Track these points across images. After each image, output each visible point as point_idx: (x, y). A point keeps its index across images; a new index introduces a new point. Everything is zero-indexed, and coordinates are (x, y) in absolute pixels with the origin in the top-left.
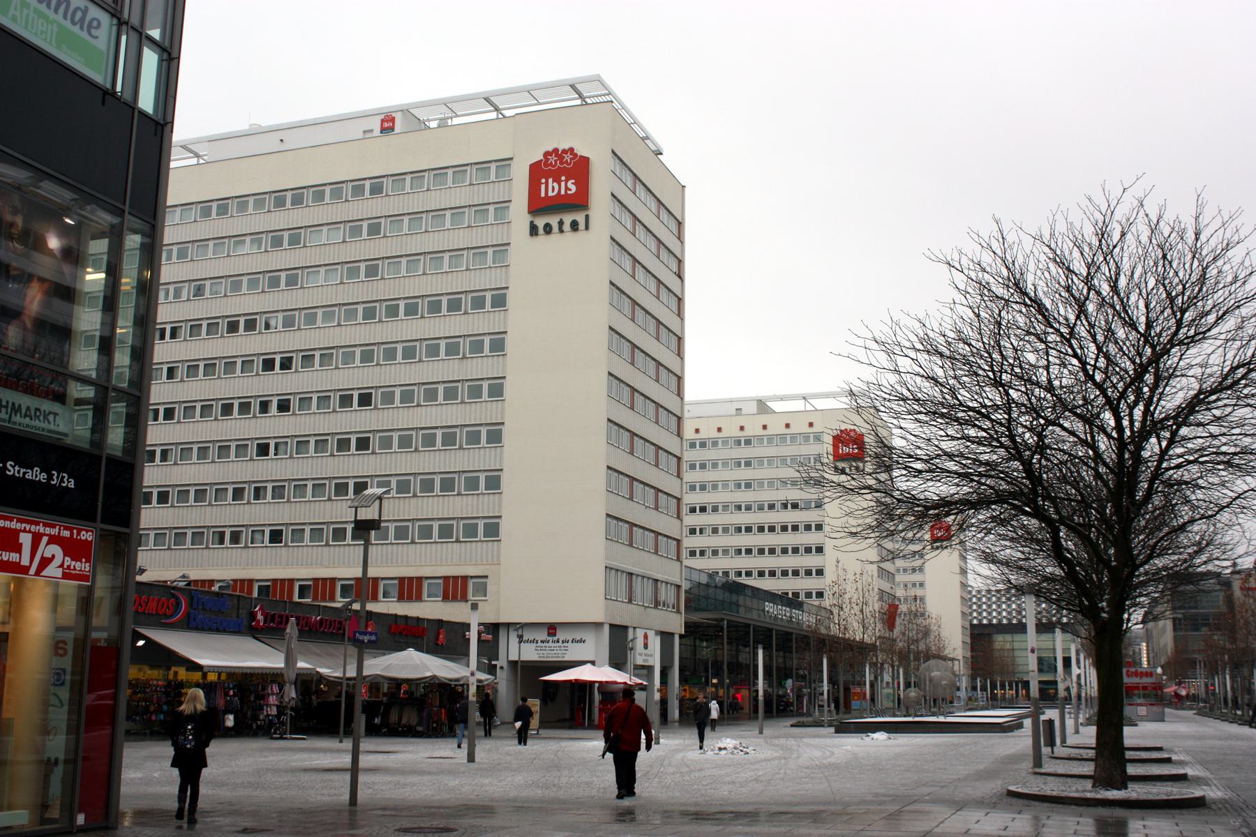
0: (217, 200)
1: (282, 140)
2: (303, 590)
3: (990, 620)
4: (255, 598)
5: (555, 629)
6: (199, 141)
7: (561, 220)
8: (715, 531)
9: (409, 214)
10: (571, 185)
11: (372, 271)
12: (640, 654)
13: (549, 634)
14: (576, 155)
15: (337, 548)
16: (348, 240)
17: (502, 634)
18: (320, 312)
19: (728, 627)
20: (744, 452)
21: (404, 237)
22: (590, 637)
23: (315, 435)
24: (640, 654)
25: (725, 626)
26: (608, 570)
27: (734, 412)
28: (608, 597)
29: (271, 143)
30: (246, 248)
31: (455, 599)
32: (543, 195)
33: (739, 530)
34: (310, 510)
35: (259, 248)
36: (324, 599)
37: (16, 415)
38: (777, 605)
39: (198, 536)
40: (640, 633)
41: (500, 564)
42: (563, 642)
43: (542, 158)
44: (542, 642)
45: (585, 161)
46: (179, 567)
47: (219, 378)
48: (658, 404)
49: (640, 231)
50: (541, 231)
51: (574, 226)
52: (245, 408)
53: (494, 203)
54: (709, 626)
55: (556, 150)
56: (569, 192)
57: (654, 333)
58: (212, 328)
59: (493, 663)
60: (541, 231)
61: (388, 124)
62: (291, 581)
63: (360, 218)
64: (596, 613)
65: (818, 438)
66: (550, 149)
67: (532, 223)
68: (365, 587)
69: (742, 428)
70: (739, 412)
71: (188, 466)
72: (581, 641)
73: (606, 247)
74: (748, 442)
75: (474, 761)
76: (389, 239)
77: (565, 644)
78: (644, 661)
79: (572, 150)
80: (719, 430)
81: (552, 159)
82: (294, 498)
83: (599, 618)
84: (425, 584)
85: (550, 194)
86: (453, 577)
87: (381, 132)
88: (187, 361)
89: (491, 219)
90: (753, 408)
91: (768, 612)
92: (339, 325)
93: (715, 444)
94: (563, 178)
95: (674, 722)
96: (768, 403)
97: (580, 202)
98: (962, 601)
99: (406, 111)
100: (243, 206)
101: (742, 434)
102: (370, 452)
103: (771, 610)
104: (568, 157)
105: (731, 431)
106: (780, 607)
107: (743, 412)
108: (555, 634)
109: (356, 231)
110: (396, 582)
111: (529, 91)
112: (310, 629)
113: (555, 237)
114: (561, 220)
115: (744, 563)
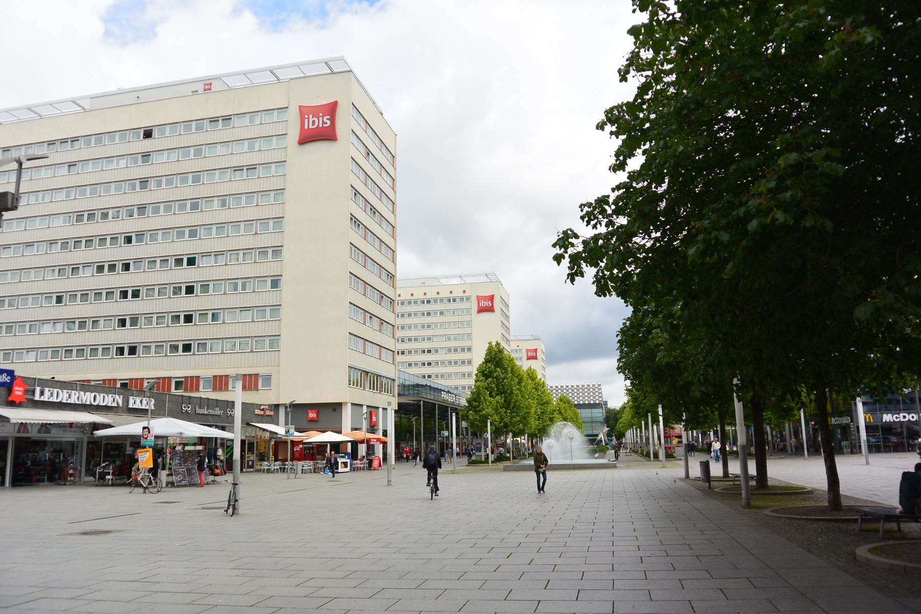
1: (138, 97)
2: (178, 385)
4: (118, 388)
6: (83, 98)
11: (196, 180)
15: (172, 358)
18: (162, 206)
20: (426, 308)
23: (158, 285)
29: (131, 99)
31: (250, 389)
34: (154, 334)
36: (191, 390)
39: (80, 351)
46: (122, 370)
48: (381, 266)
52: (112, 268)
56: (324, 125)
57: (378, 248)
58: (91, 216)
61: (208, 87)
62: (170, 378)
65: (468, 299)
68: (192, 383)
71: (74, 306)
74: (429, 302)
82: (144, 326)
85: (311, 127)
86: (135, 379)
91: (443, 397)
93: (410, 303)
99: (218, 78)
103: (445, 396)
107: (426, 284)
111: (298, 65)
115: (427, 370)
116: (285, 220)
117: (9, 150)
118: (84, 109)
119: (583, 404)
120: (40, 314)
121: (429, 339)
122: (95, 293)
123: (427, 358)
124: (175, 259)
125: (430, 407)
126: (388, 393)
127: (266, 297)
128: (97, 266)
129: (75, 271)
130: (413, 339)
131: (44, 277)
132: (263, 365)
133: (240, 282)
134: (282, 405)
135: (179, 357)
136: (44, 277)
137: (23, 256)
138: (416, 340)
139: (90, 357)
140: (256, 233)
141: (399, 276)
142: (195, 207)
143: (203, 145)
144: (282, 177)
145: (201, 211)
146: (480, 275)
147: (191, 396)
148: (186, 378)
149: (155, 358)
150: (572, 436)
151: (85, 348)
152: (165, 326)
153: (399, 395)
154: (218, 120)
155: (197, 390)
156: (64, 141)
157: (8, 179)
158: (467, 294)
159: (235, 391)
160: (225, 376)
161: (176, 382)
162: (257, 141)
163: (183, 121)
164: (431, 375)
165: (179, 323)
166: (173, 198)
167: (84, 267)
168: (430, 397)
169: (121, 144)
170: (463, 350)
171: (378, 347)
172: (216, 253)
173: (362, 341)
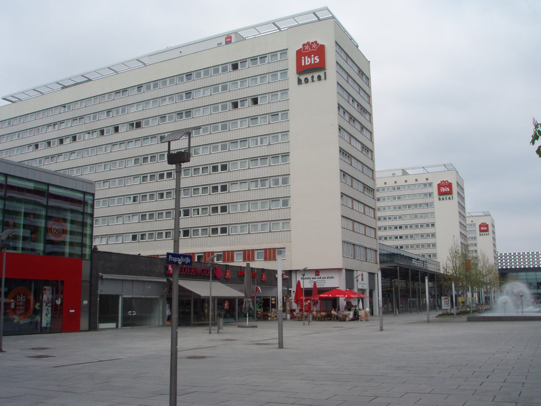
0: (153, 81)
1: (181, 52)
3: (511, 267)
5: (319, 272)
6: (144, 57)
7: (313, 75)
8: (385, 229)
9: (240, 79)
10: (448, 189)
12: (360, 283)
13: (316, 275)
14: (318, 44)
16: (212, 94)
17: (293, 275)
19: (400, 270)
20: (396, 193)
21: (239, 90)
22: (336, 276)
24: (360, 283)
25: (398, 270)
26: (343, 243)
27: (392, 175)
28: (344, 256)
29: (177, 54)
30: (167, 102)
31: (270, 259)
32: (303, 64)
33: (396, 228)
35: (173, 101)
36: (228, 261)
41: (291, 242)
42: (323, 278)
43: (302, 47)
44: (313, 278)
45: (322, 47)
47: (157, 162)
49: (350, 80)
50: (303, 81)
51: (319, 78)
53: (280, 71)
55: (308, 43)
59: (290, 289)
60: (303, 81)
61: (228, 39)
63: (218, 83)
64: (339, 264)
65: (431, 184)
66: (305, 42)
67: (298, 78)
68: (229, 255)
69: (396, 182)
70: (394, 175)
71: (145, 203)
72: (332, 278)
73: (334, 88)
74: (399, 188)
75: (282, 347)
76: (232, 92)
77: (324, 279)
78: (362, 287)
79: (316, 42)
80: (385, 183)
81: (443, 183)
83: (340, 267)
84: (256, 253)
85: (307, 64)
87: (226, 44)
88: (143, 155)
89: (279, 78)
90: (400, 173)
91: (414, 263)
92: (210, 134)
93: (384, 190)
94: (313, 56)
95: (376, 316)
96: (407, 171)
97: (321, 66)
98: (494, 258)
99: (236, 33)
100: (164, 84)
101: (395, 185)
102: (227, 192)
103: (415, 263)
104: (314, 46)
105: (391, 183)
107: (396, 175)
108: (319, 275)
109: (216, 90)
110: (242, 252)
111: (293, 17)
112: (197, 274)
113: (445, 201)
114: (313, 75)
115: (399, 242)
116: (290, 133)
117: (127, 90)
118: (144, 64)
119: (519, 268)
120: (123, 210)
121: (400, 218)
122: (194, 189)
123: (399, 232)
124: (212, 166)
125: (403, 271)
128: (159, 174)
129: (204, 170)
130: (387, 218)
131: (125, 184)
132: (279, 242)
133: (280, 179)
134: (294, 271)
135: (218, 237)
136: (125, 184)
137: (110, 170)
138: (390, 218)
139: (158, 239)
140: (269, 144)
141: (377, 169)
142: (224, 127)
143: (227, 82)
144: (286, 101)
145: (229, 130)
146: (440, 166)
147: (229, 264)
148: (224, 252)
149: (201, 238)
150: (522, 294)
151: (208, 228)
152: (208, 215)
153: (381, 262)
154: (257, 59)
155: (232, 260)
156: (117, 92)
157: (85, 121)
158: (429, 181)
159: (285, 259)
160: (251, 250)
161: (198, 256)
163: (213, 66)
164: (403, 246)
165: (218, 213)
166: (208, 122)
167: (104, 182)
168: (403, 263)
169: (171, 87)
170: (428, 225)
171: (363, 226)
173: (351, 222)
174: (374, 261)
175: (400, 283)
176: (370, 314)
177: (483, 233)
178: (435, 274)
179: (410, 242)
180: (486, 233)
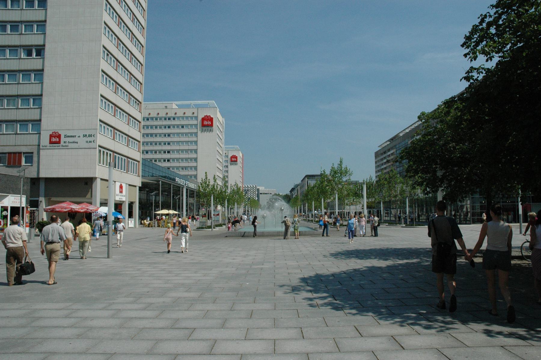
25: (161, 184)
37: (500, 57)
38: (181, 179)
40: (118, 185)
45: (212, 118)
51: (210, 131)
54: (416, 263)
55: (207, 116)
74: (169, 119)
91: (177, 181)
103: (178, 181)
106: (181, 180)
107: (168, 108)
115: (167, 164)
126: (134, 173)
127: (34, 63)
162: (310, 183)
172: (27, 24)
174: (136, 174)
175: (231, 210)
176: (69, 210)
177: (233, 163)
178: (194, 191)
179: (158, 156)
180: (235, 163)
